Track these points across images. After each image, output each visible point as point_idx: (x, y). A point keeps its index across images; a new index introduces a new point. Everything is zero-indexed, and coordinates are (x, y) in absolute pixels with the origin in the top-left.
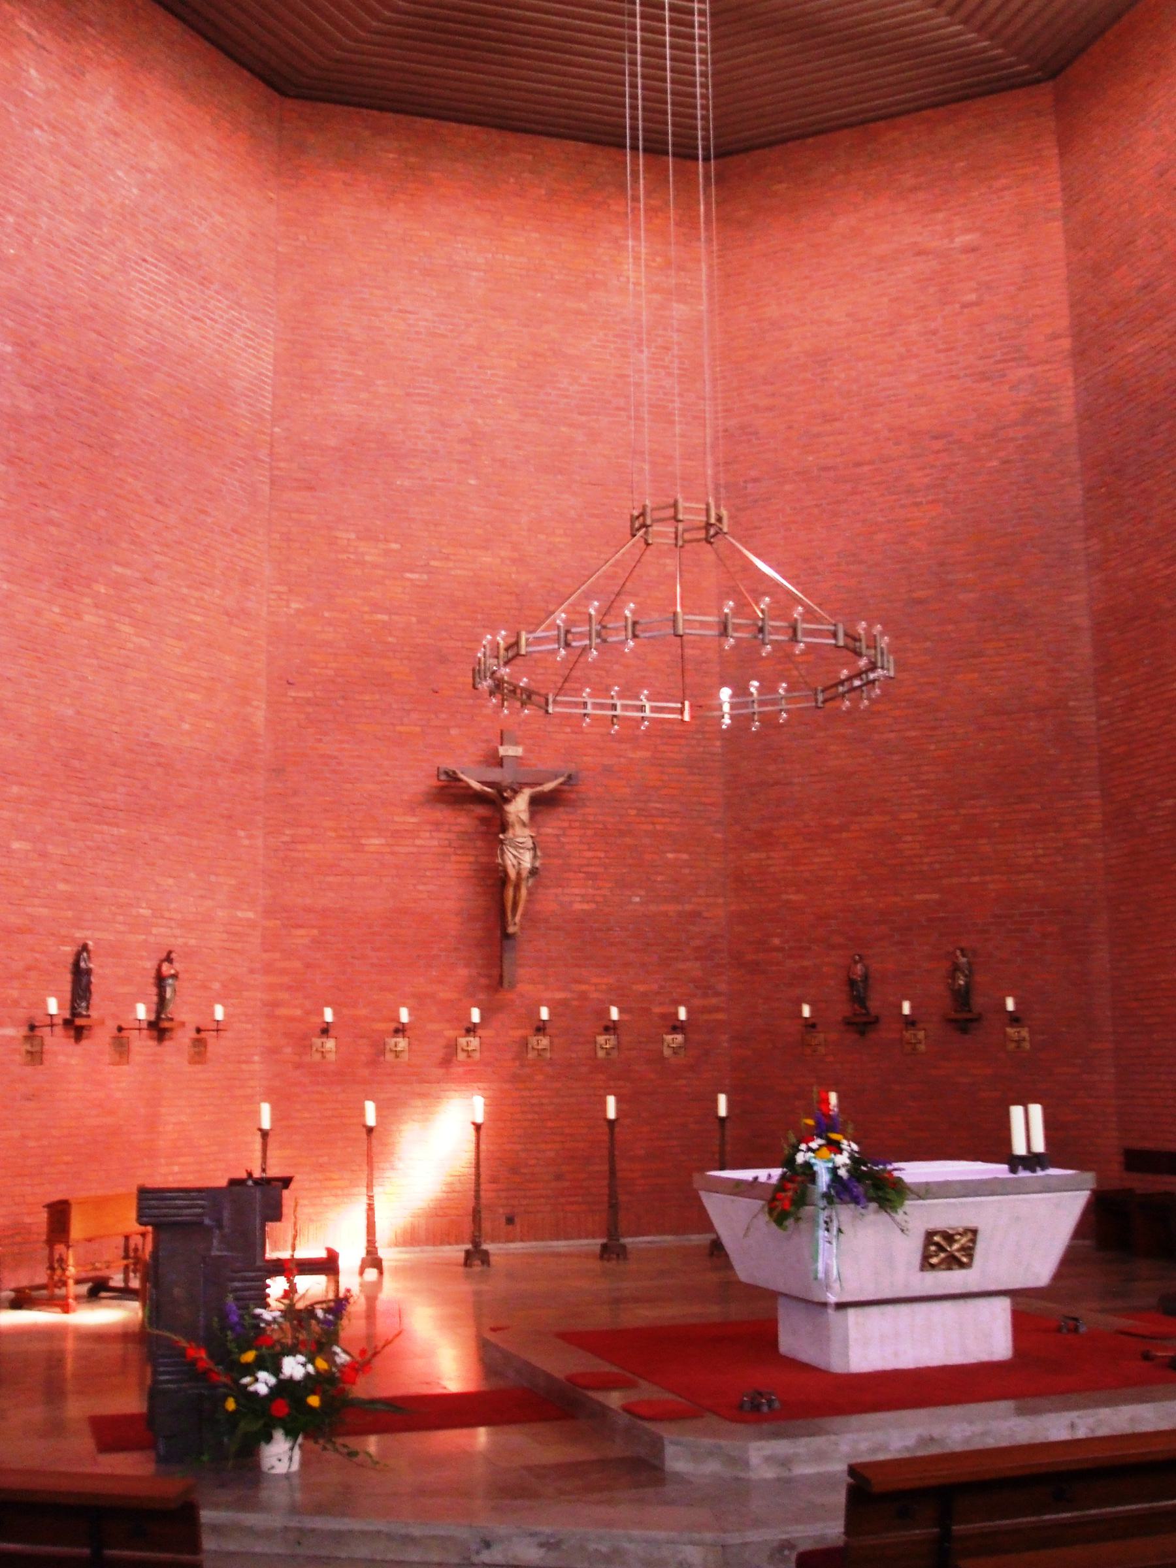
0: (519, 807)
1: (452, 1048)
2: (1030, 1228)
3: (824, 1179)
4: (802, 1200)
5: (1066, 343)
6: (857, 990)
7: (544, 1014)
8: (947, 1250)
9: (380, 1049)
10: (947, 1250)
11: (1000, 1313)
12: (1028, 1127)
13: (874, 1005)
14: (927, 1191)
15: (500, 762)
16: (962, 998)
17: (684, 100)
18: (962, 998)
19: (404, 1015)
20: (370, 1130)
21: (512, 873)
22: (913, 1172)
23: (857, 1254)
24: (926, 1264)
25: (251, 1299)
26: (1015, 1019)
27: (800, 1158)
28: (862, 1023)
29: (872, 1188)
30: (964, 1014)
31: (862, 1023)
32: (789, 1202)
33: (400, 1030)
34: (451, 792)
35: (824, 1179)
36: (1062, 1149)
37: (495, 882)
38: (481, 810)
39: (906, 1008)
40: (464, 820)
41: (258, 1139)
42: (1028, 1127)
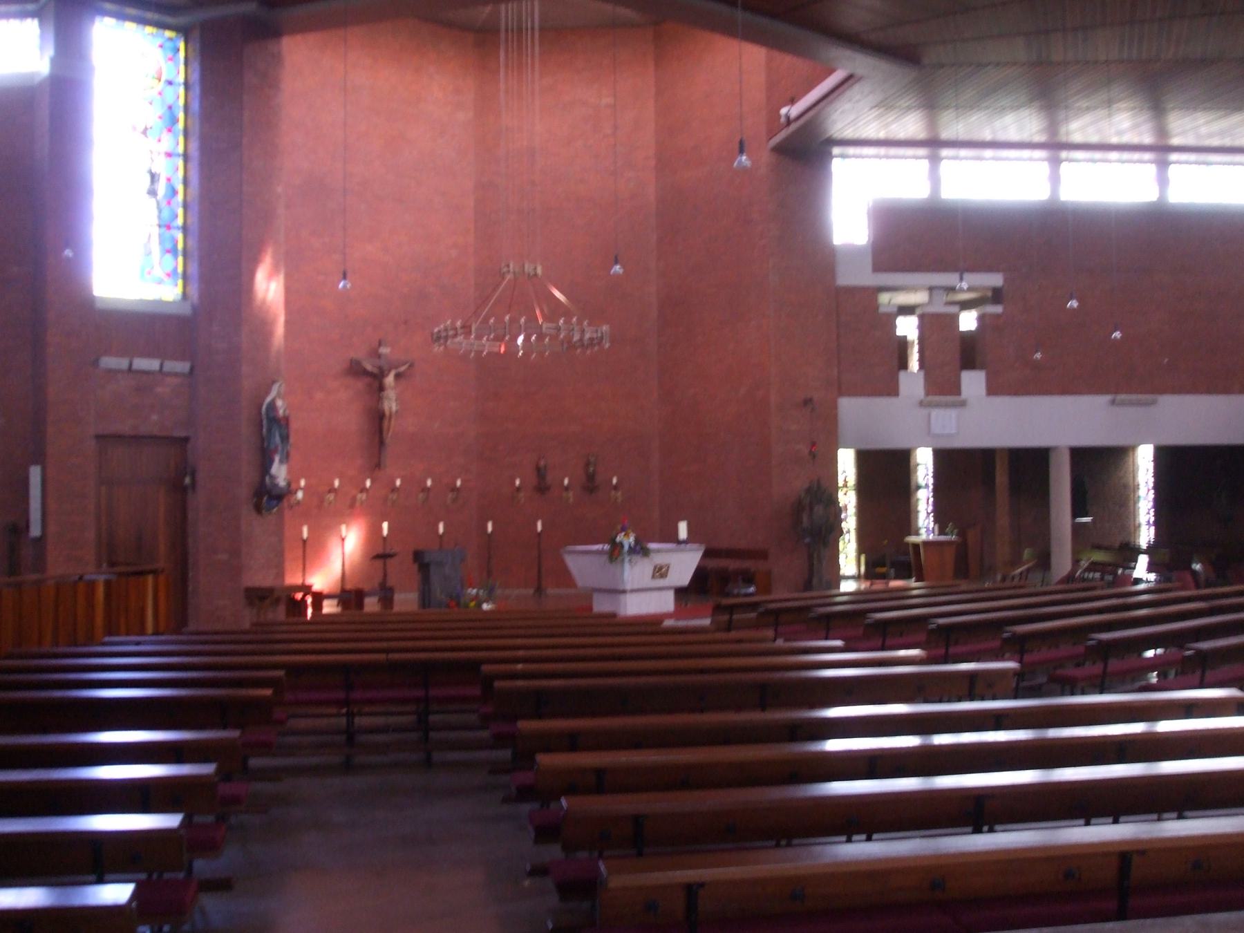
0: (390, 380)
1: (354, 499)
2: (684, 564)
3: (626, 547)
4: (620, 553)
5: (653, 163)
6: (540, 472)
7: (398, 483)
8: (661, 572)
9: (322, 501)
10: (661, 572)
11: (670, 595)
12: (683, 530)
13: (549, 479)
14: (658, 551)
15: (379, 356)
16: (591, 477)
17: (507, 52)
18: (591, 477)
19: (337, 483)
20: (304, 542)
21: (387, 413)
22: (652, 546)
23: (635, 572)
24: (653, 577)
25: (282, 624)
26: (616, 488)
27: (618, 539)
28: (542, 488)
29: (640, 550)
30: (590, 484)
31: (542, 488)
32: (615, 552)
33: (332, 490)
34: (355, 370)
35: (626, 547)
36: (693, 537)
37: (377, 420)
38: (368, 380)
39: (566, 482)
40: (361, 384)
41: (301, 544)
42: (683, 530)
